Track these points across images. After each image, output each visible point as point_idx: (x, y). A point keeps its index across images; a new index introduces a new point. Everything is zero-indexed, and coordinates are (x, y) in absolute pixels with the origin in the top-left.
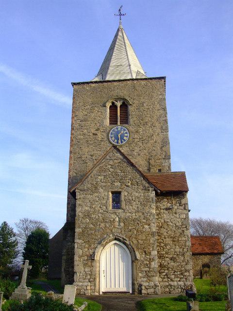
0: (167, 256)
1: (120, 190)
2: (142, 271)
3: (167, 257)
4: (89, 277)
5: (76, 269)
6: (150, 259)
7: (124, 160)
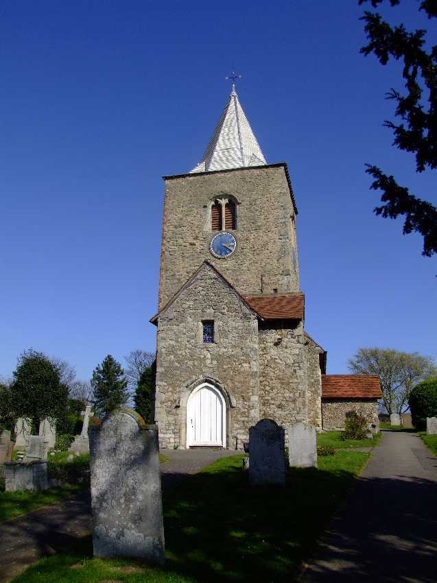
0: (273, 402)
1: (213, 319)
2: (239, 421)
3: (273, 404)
4: (173, 427)
5: (157, 417)
6: (249, 406)
7: (220, 279)
